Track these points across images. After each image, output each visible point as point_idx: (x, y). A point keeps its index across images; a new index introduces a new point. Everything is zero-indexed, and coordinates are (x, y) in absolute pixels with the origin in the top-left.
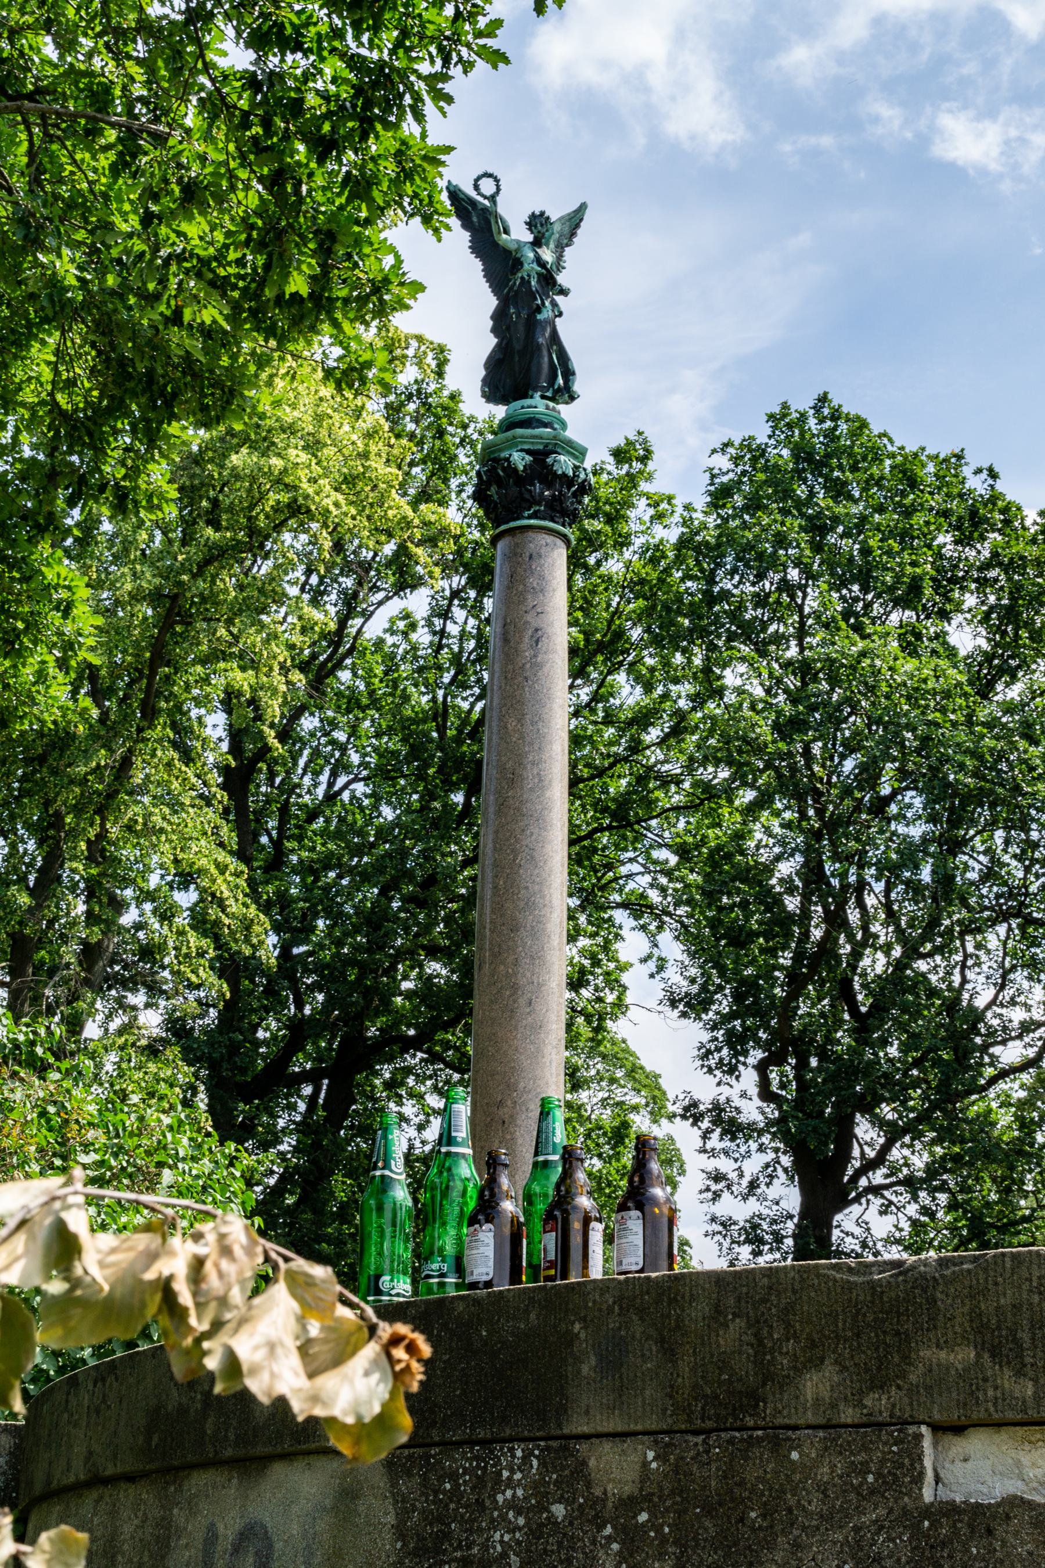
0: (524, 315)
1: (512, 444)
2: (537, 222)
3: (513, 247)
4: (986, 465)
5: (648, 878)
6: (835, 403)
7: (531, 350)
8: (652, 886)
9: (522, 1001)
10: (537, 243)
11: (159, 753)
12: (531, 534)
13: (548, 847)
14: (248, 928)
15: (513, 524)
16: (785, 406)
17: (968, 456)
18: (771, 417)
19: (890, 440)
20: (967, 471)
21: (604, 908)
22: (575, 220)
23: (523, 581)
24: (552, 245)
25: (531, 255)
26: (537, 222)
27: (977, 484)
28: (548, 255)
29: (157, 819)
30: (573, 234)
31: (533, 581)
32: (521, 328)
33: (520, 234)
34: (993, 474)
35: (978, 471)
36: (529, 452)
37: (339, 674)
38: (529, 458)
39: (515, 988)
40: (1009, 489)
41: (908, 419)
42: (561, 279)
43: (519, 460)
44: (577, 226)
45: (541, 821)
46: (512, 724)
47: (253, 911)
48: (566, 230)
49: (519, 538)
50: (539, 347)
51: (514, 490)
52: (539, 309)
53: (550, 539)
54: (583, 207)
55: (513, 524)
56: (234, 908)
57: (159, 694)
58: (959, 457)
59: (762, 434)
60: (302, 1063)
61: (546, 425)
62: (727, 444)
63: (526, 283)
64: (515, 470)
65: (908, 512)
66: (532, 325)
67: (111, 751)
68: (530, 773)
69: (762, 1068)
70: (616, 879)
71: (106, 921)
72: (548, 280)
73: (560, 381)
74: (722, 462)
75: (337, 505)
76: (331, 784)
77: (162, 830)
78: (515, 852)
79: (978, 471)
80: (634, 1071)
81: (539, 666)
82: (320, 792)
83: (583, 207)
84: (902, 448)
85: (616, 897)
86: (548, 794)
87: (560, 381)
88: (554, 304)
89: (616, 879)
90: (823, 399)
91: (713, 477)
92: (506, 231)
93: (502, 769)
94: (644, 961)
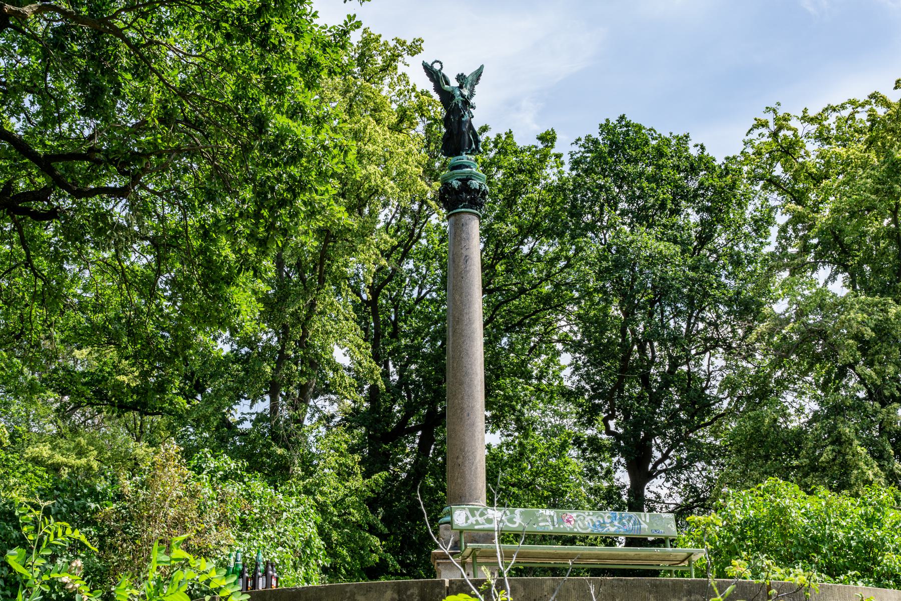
0: (457, 119)
1: (452, 176)
2: (460, 78)
3: (450, 90)
4: (700, 143)
5: (568, 327)
6: (628, 119)
7: (461, 134)
8: (571, 331)
9: (465, 414)
10: (461, 87)
11: (327, 299)
12: (463, 215)
13: (474, 349)
14: (372, 372)
15: (455, 211)
16: (607, 120)
17: (691, 136)
18: (601, 126)
19: (655, 132)
20: (691, 144)
21: (550, 342)
22: (478, 74)
23: (460, 236)
24: (468, 86)
25: (458, 93)
26: (460, 78)
27: (694, 152)
28: (466, 92)
29: (329, 328)
30: (478, 79)
31: (464, 235)
32: (456, 124)
33: (454, 83)
34: (703, 148)
35: (696, 146)
36: (459, 180)
37: (420, 240)
38: (460, 183)
39: (462, 409)
40: (709, 151)
41: (660, 122)
42: (472, 101)
43: (456, 184)
44: (480, 75)
45: (471, 338)
46: (457, 297)
47: (374, 364)
48: (475, 78)
49: (457, 217)
50: (464, 133)
51: (455, 197)
52: (463, 116)
53: (471, 216)
54: (482, 67)
55: (455, 211)
56: (365, 364)
57: (325, 272)
58: (687, 137)
59: (596, 134)
60: (413, 422)
61: (467, 167)
62: (579, 139)
63: (456, 105)
64: (454, 188)
65: (659, 167)
66: (460, 123)
67: (306, 300)
68: (466, 317)
69: (605, 421)
70: (554, 329)
71: (309, 374)
72: (466, 103)
73: (474, 146)
74: (576, 148)
75: (392, 188)
76: (419, 293)
77: (331, 332)
78: (460, 352)
79: (696, 146)
80: (444, 475)
81: (468, 272)
82: (415, 295)
83: (482, 67)
84: (660, 135)
85: (555, 337)
86: (474, 326)
87: (474, 146)
88: (470, 113)
89: (554, 329)
90: (622, 118)
91: (572, 155)
92: (447, 83)
93: (454, 317)
94: (570, 365)
